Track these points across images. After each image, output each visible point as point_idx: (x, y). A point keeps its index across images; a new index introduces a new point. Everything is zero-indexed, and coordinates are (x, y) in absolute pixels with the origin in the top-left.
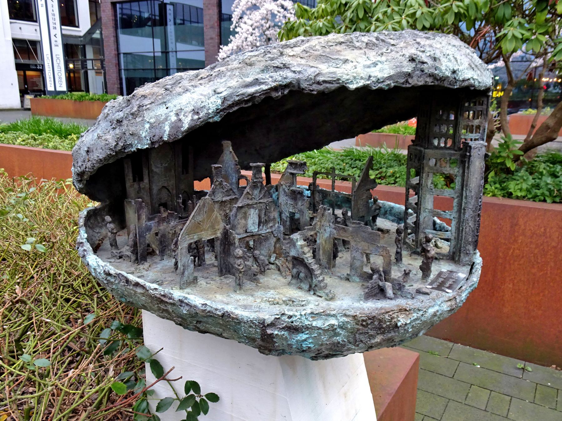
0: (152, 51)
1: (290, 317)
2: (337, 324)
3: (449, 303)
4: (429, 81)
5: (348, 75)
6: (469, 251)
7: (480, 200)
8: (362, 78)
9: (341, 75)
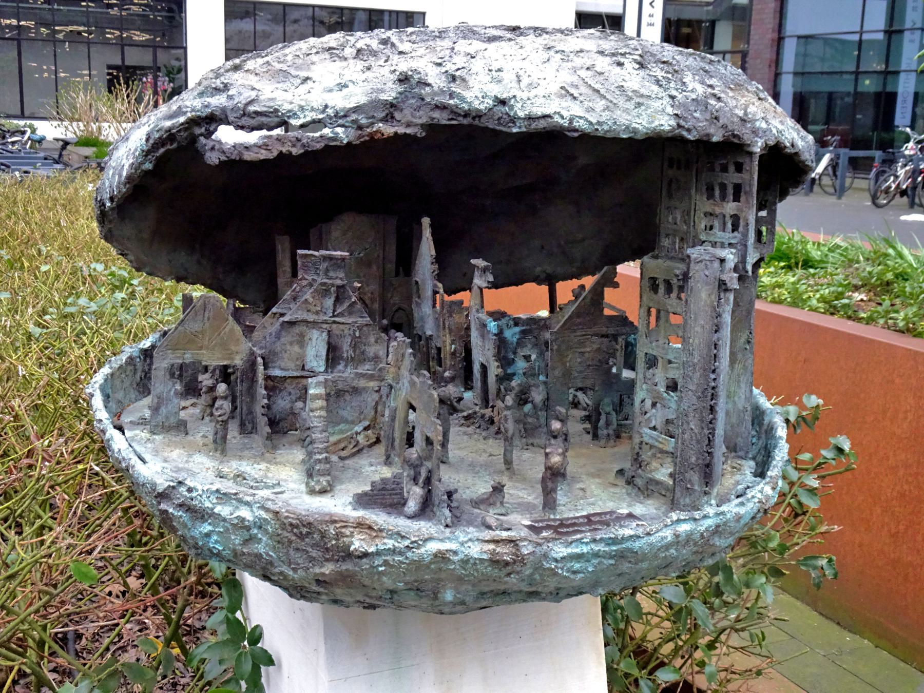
0: (858, 29)
1: (190, 490)
2: (251, 519)
3: (491, 547)
4: (441, 118)
5: (291, 103)
6: (692, 485)
7: (713, 376)
8: (313, 109)
9: (279, 103)
